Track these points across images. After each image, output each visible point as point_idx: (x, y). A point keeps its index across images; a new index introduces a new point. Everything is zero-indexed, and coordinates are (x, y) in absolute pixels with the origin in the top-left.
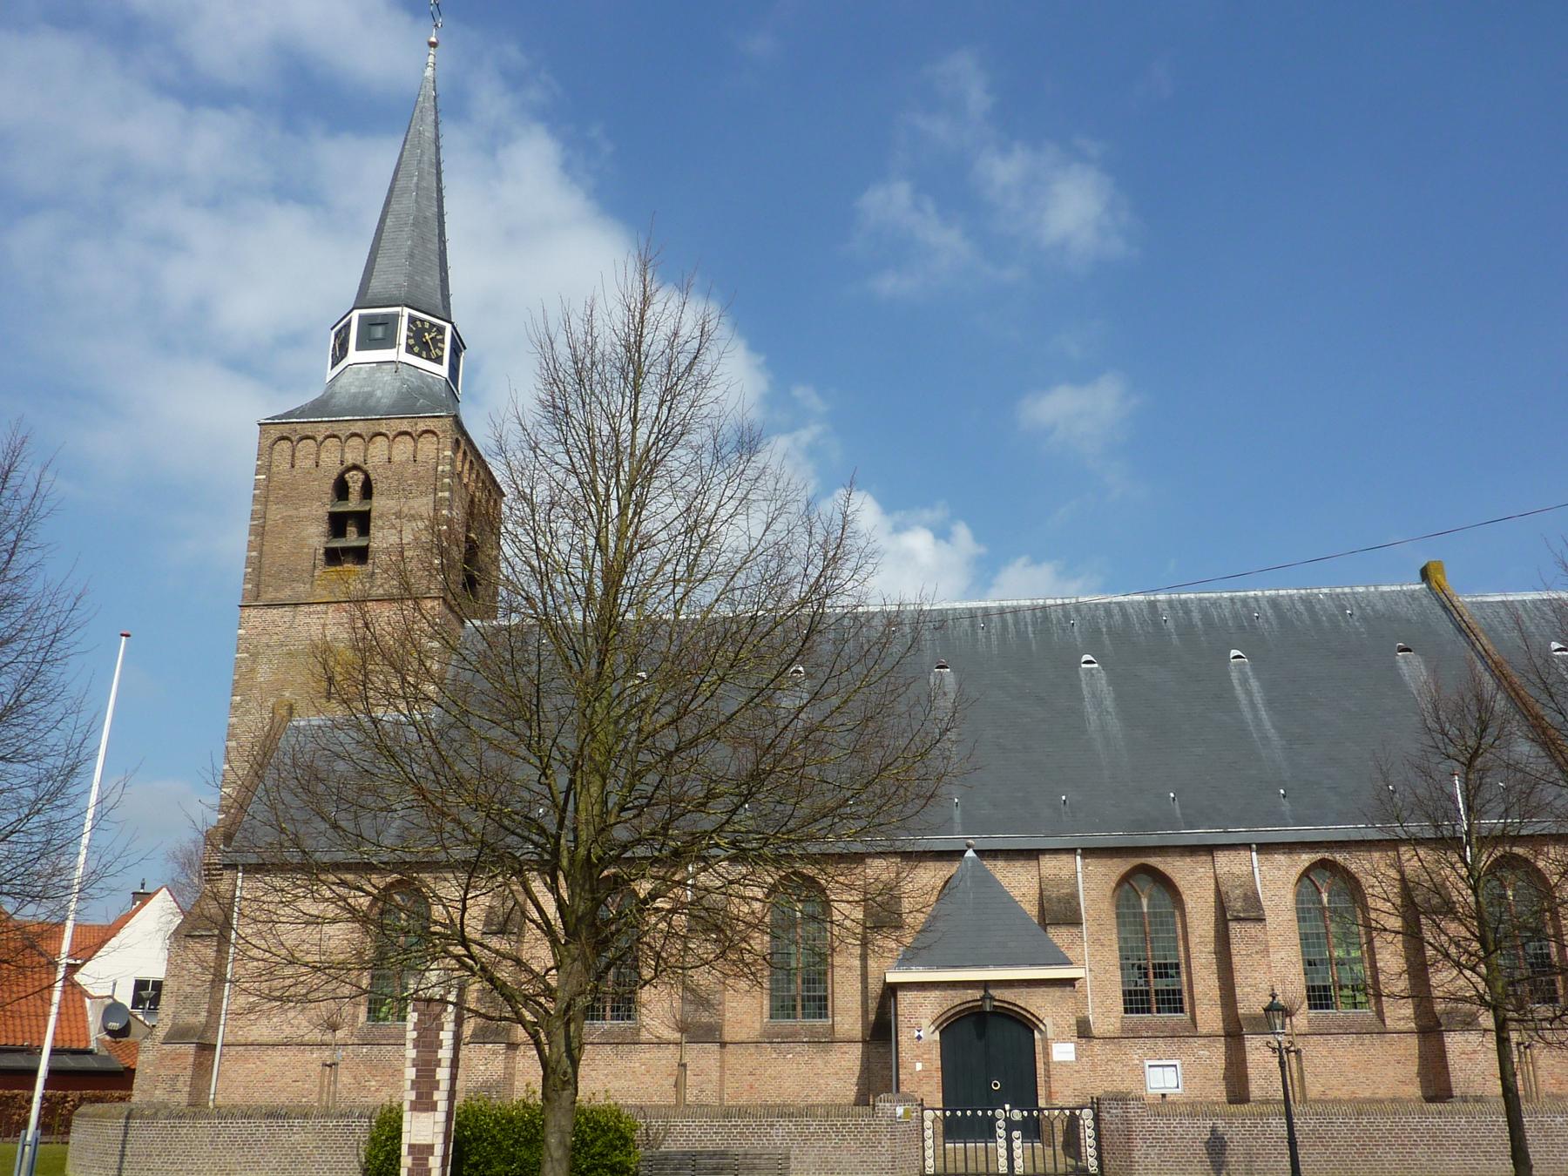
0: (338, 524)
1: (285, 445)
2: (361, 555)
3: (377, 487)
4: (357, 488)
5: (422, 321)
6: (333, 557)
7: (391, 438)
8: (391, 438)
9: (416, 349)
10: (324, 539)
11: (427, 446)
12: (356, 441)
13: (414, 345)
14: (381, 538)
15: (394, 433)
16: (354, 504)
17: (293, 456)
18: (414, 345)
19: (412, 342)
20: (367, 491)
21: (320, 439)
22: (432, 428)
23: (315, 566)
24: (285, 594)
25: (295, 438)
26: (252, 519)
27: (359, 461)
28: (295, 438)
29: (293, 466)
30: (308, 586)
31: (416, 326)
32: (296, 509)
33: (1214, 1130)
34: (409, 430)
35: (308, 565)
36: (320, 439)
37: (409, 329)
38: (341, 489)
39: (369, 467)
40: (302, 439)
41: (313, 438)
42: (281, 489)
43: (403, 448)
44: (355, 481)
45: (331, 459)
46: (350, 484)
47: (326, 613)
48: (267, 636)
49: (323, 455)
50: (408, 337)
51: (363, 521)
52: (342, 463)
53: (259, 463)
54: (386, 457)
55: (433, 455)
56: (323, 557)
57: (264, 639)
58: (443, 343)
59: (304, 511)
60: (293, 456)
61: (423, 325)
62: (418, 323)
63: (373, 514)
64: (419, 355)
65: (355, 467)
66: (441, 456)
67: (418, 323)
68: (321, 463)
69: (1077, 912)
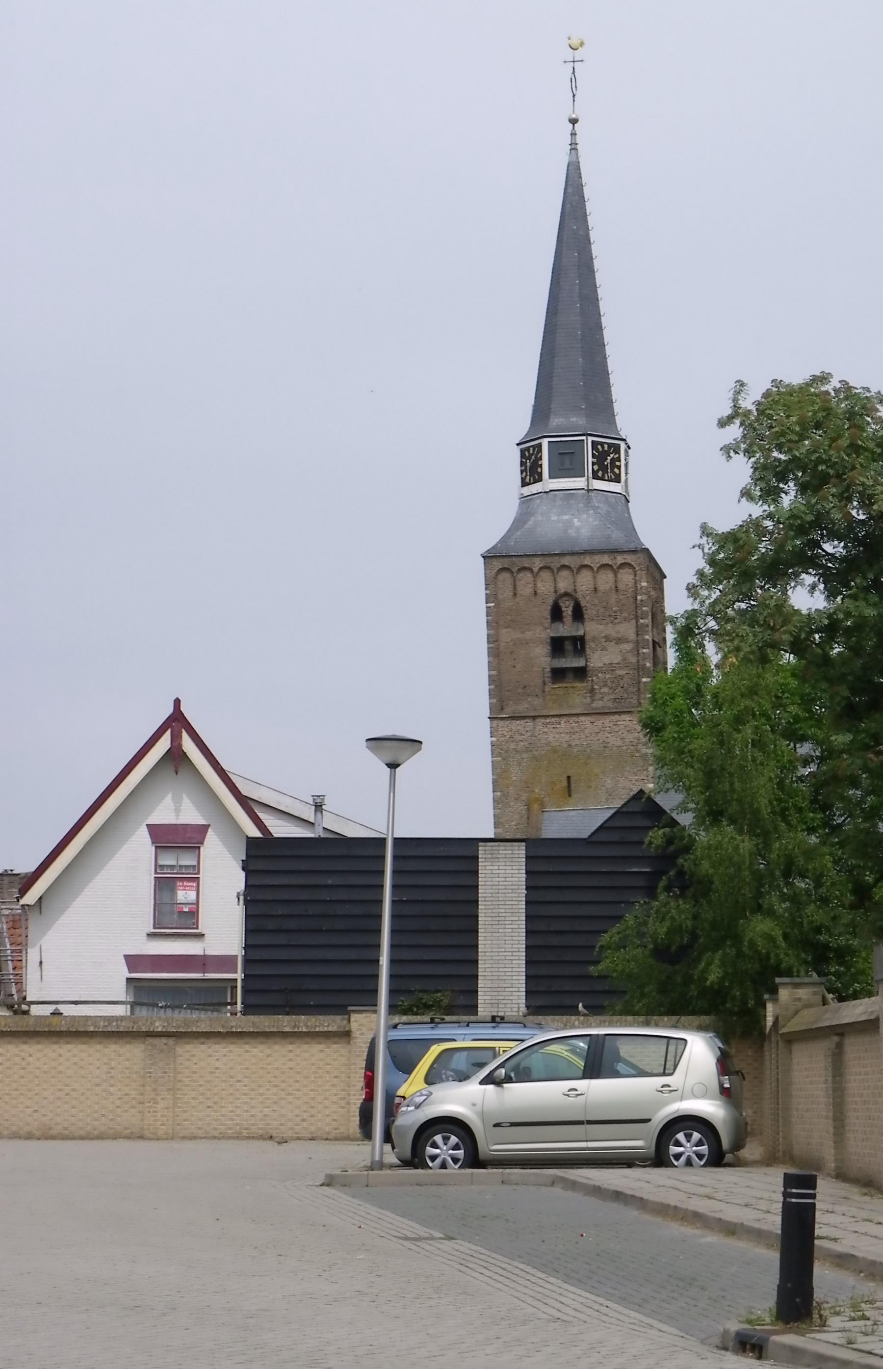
0: (557, 646)
1: (506, 576)
2: (581, 673)
3: (588, 613)
4: (570, 613)
5: (602, 444)
6: (558, 674)
7: (595, 569)
8: (595, 569)
9: (600, 474)
10: (549, 659)
11: (626, 577)
12: (565, 573)
13: (598, 471)
14: (597, 659)
15: (598, 565)
16: (566, 629)
17: (515, 586)
18: (598, 471)
19: (596, 467)
20: (578, 614)
21: (536, 570)
22: (629, 561)
23: (544, 683)
24: (523, 708)
25: (515, 569)
26: (488, 642)
27: (570, 590)
28: (515, 569)
29: (515, 594)
30: (541, 700)
31: (597, 450)
32: (523, 633)
33: (147, 825)
34: (610, 563)
35: (539, 682)
36: (536, 570)
37: (593, 456)
38: (556, 614)
39: (579, 595)
40: (520, 570)
41: (530, 569)
42: (507, 614)
43: (606, 580)
44: (568, 610)
45: (546, 586)
46: (564, 609)
47: (560, 724)
48: (515, 743)
49: (539, 585)
50: (593, 464)
51: (579, 644)
52: (556, 591)
53: (488, 592)
54: (592, 586)
55: (631, 584)
56: (549, 675)
57: (512, 746)
58: (620, 461)
59: (529, 635)
60: (515, 586)
61: (603, 447)
62: (599, 447)
63: (587, 638)
64: (602, 479)
65: (566, 594)
66: (639, 586)
67: (599, 447)
68: (538, 591)
69: (597, 1076)
